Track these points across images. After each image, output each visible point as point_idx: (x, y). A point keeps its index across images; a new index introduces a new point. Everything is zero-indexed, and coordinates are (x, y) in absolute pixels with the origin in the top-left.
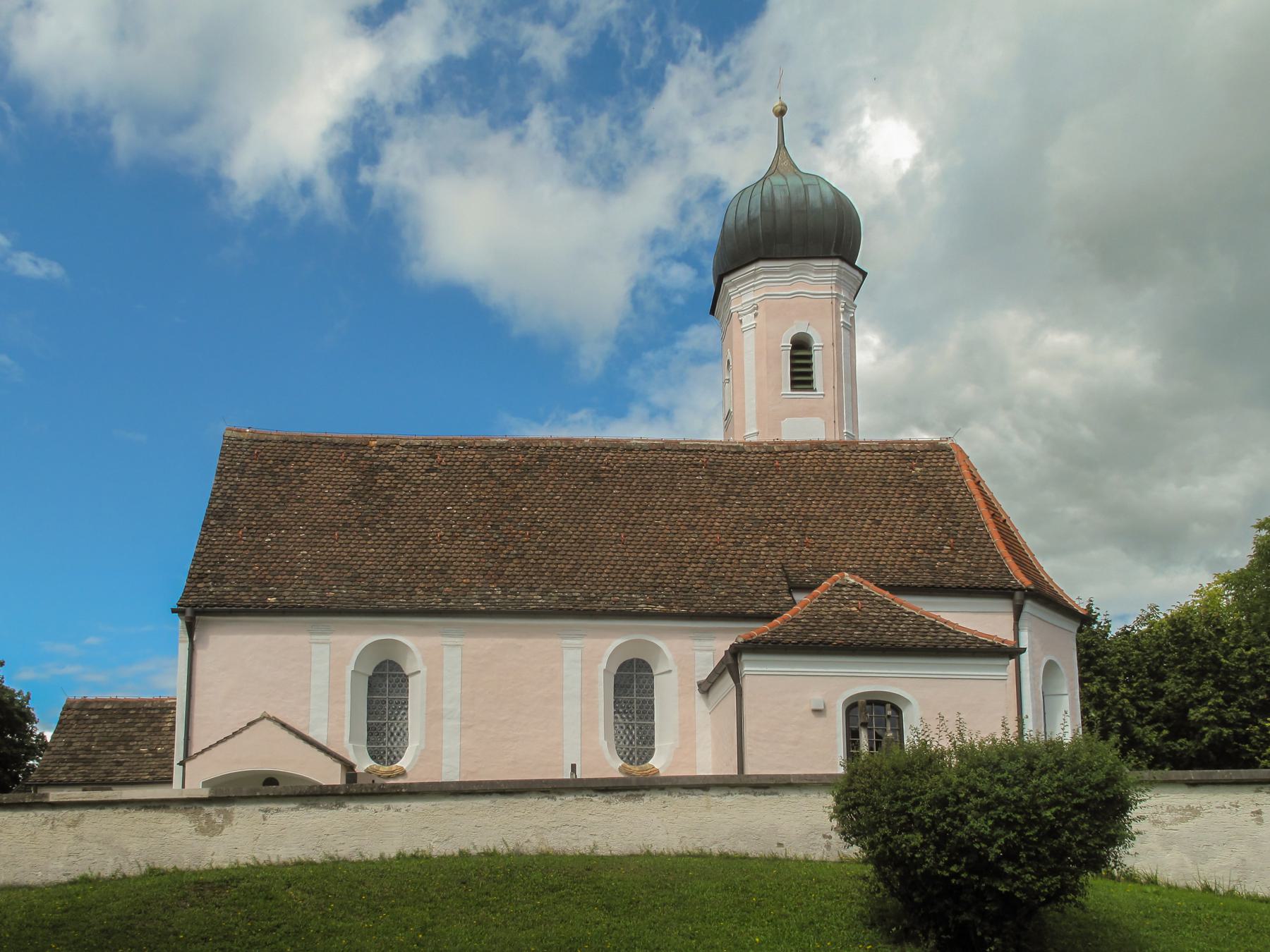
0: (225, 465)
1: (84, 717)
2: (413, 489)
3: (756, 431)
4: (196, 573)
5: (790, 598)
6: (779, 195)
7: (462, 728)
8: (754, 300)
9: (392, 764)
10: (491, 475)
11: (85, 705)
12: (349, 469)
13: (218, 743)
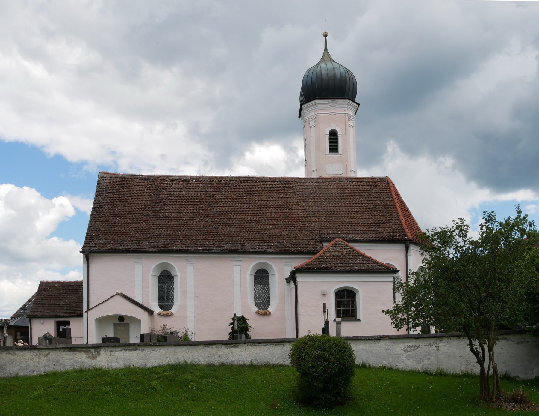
0: (99, 189)
1: (47, 289)
2: (175, 199)
3: (316, 169)
4: (89, 235)
5: (321, 245)
6: (324, 72)
7: (195, 297)
8: (314, 115)
9: (168, 310)
10: (206, 193)
11: (47, 283)
12: (149, 190)
13: (100, 304)
